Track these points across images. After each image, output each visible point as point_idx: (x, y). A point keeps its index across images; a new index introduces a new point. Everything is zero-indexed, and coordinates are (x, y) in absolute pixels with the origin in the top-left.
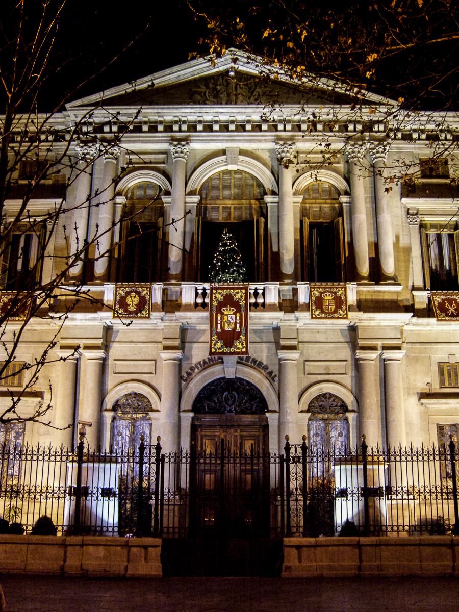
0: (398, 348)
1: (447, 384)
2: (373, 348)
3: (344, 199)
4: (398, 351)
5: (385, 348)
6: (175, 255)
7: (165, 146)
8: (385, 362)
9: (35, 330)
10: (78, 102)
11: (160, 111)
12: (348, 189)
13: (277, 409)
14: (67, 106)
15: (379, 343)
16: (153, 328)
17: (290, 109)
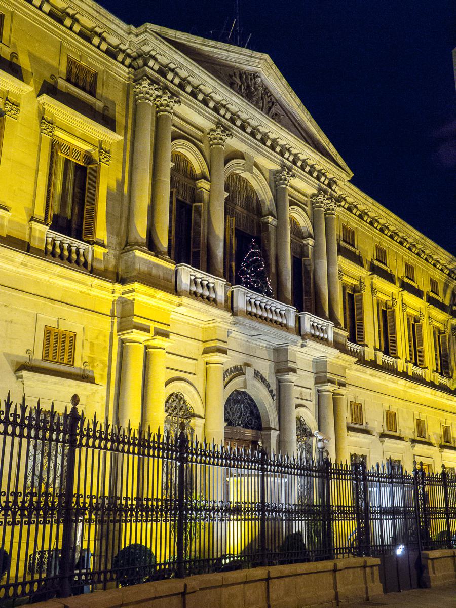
0: (166, 335)
1: (50, 357)
2: (146, 330)
3: (311, 242)
4: (225, 355)
5: (158, 333)
6: (219, 252)
7: (207, 125)
8: (320, 393)
9: (89, 295)
10: (157, 28)
11: (218, 87)
12: (312, 232)
13: (202, 415)
14: (149, 26)
15: (153, 326)
16: (196, 324)
17: (153, 38)
